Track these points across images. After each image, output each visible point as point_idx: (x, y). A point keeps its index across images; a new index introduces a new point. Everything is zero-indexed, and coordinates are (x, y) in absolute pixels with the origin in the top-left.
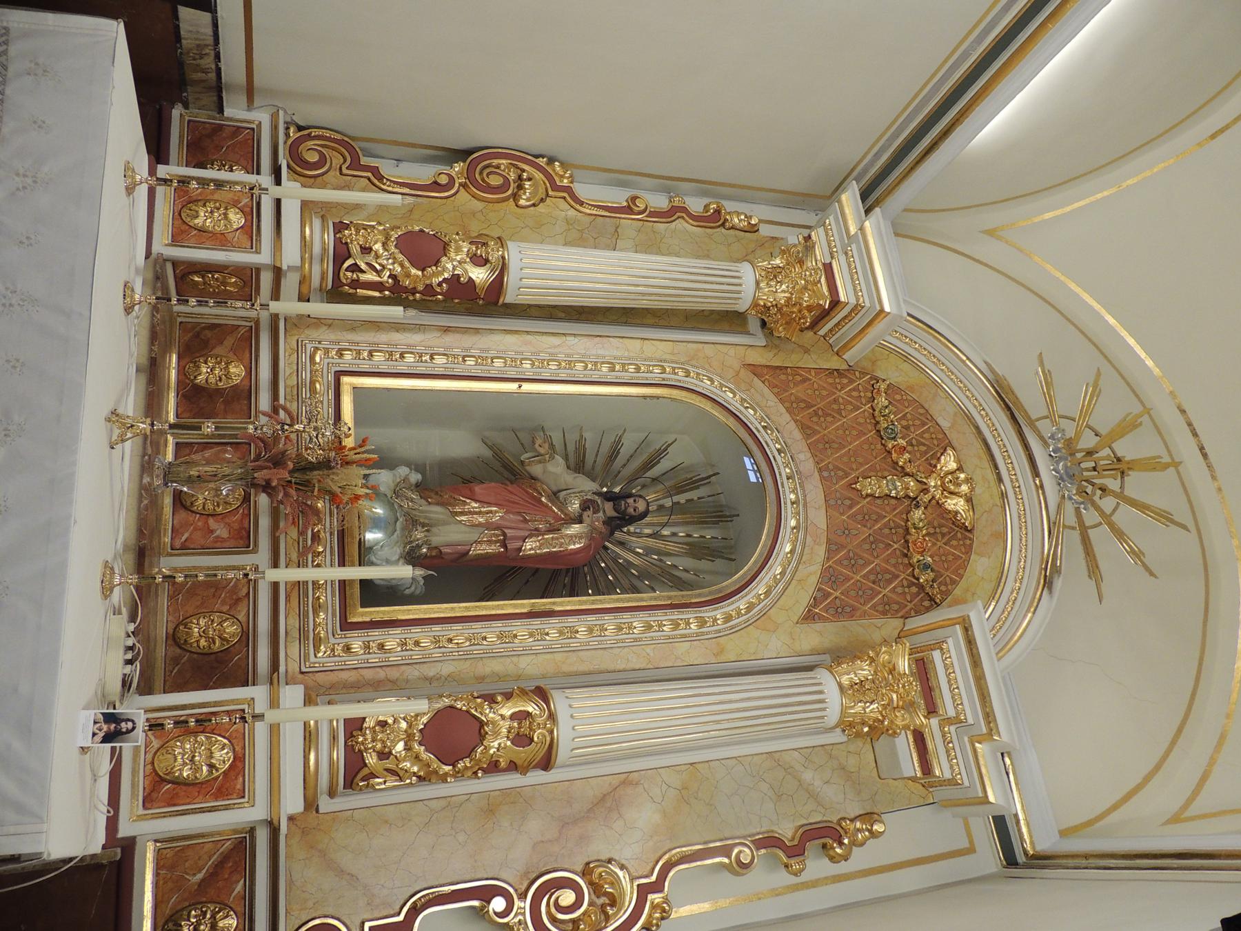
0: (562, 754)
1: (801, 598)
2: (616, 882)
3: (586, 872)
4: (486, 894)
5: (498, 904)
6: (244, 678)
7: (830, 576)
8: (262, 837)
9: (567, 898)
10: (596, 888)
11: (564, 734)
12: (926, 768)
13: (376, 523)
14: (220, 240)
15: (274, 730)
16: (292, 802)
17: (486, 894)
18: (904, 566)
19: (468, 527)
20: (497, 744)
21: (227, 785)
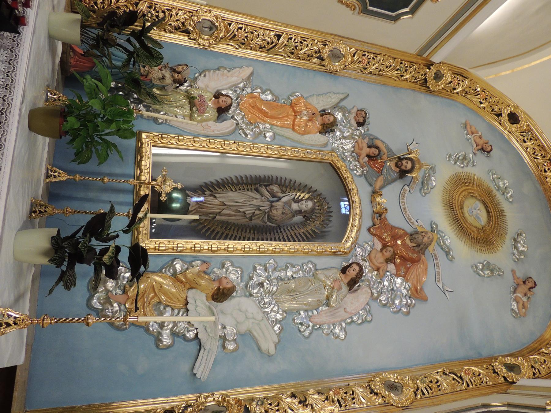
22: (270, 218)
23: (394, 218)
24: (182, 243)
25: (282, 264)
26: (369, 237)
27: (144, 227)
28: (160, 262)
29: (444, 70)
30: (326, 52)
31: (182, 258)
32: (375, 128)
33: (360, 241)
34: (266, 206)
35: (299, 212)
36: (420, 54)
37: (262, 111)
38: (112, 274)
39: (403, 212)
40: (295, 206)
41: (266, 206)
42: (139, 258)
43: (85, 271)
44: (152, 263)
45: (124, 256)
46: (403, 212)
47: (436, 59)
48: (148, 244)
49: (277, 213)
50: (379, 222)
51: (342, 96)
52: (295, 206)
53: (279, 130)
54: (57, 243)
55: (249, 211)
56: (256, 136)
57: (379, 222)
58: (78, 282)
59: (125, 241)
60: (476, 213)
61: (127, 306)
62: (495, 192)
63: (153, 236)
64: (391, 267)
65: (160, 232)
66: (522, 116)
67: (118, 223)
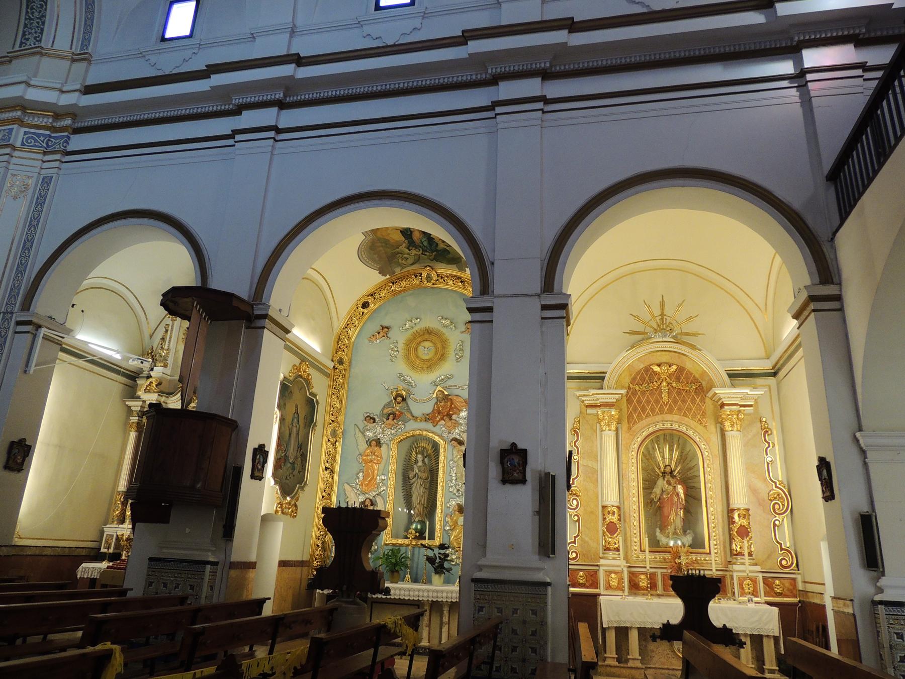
0: (746, 507)
1: (700, 428)
2: (774, 494)
3: (772, 501)
4: (775, 525)
5: (777, 523)
6: (596, 572)
7: (694, 417)
8: (765, 575)
9: (777, 506)
10: (775, 498)
11: (742, 506)
12: (751, 406)
13: (675, 543)
14: (621, 580)
15: (750, 572)
16: (758, 568)
17: (775, 525)
18: (691, 389)
19: (676, 517)
20: (744, 522)
21: (754, 581)
22: (426, 479)
23: (428, 408)
24: (438, 526)
25: (449, 478)
26: (438, 426)
27: (431, 543)
28: (446, 536)
29: (337, 358)
30: (332, 440)
31: (444, 526)
32: (376, 411)
33: (440, 432)
34: (420, 481)
35: (423, 461)
36: (328, 375)
37: (370, 481)
38: (447, 555)
39: (425, 401)
40: (420, 463)
41: (420, 481)
42: (442, 546)
43: (446, 565)
44: (446, 542)
45: (442, 551)
46: (425, 401)
47: (331, 365)
48: (437, 542)
49: (424, 475)
50: (429, 418)
51: (357, 430)
52: (420, 463)
53: (380, 473)
54: (437, 572)
55: (422, 490)
56: (384, 485)
57: (429, 418)
58: (162, 311)
59: (437, 551)
60: (426, 350)
61: (680, 489)
62: (414, 330)
63: (433, 539)
64: (454, 417)
65: (432, 537)
66: (363, 300)
67: (430, 553)
